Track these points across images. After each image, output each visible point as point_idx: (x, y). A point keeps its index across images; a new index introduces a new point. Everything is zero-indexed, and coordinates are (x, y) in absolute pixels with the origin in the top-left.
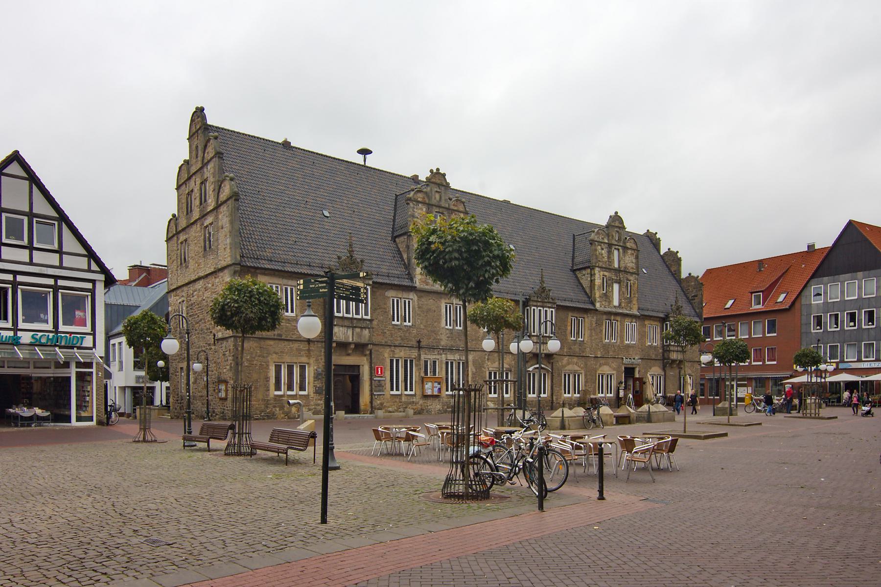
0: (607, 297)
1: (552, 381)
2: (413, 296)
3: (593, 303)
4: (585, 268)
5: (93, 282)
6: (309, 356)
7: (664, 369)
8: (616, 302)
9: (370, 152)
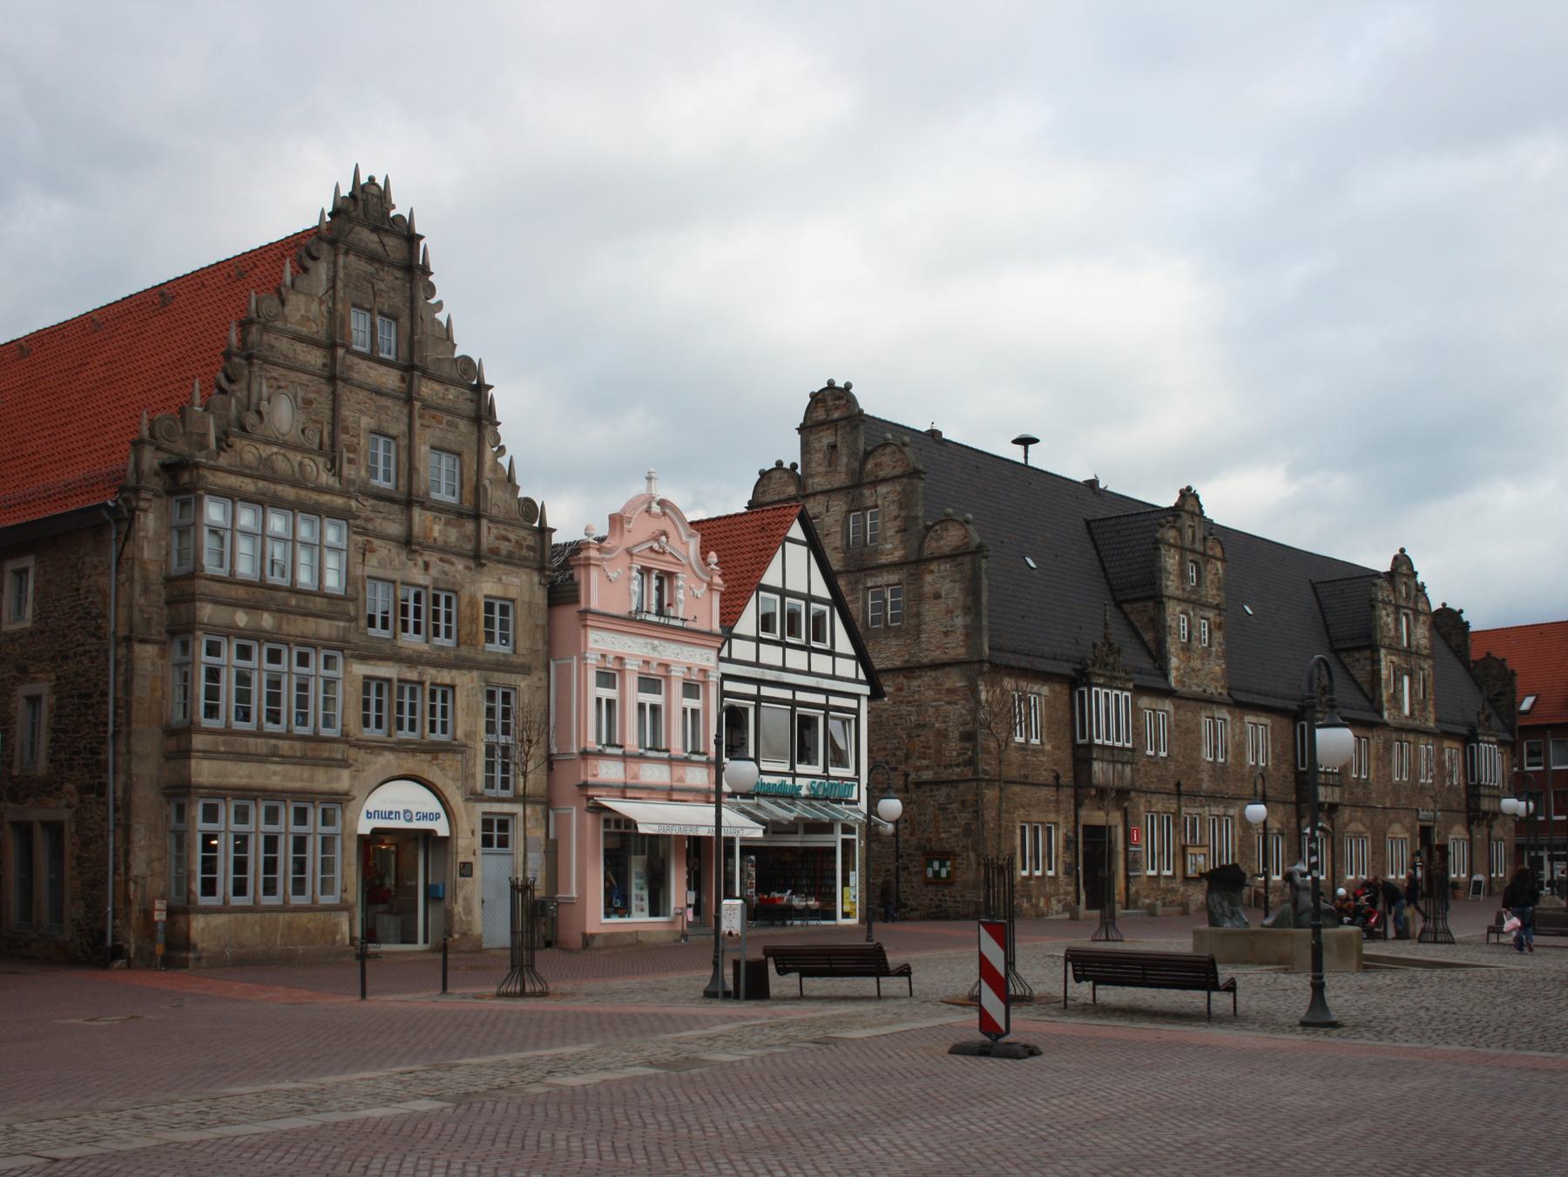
0: (1396, 699)
1: (1333, 852)
2: (1168, 705)
3: (1379, 712)
4: (1359, 649)
5: (856, 696)
6: (1057, 812)
7: (1469, 831)
8: (1407, 711)
9: (1035, 441)
